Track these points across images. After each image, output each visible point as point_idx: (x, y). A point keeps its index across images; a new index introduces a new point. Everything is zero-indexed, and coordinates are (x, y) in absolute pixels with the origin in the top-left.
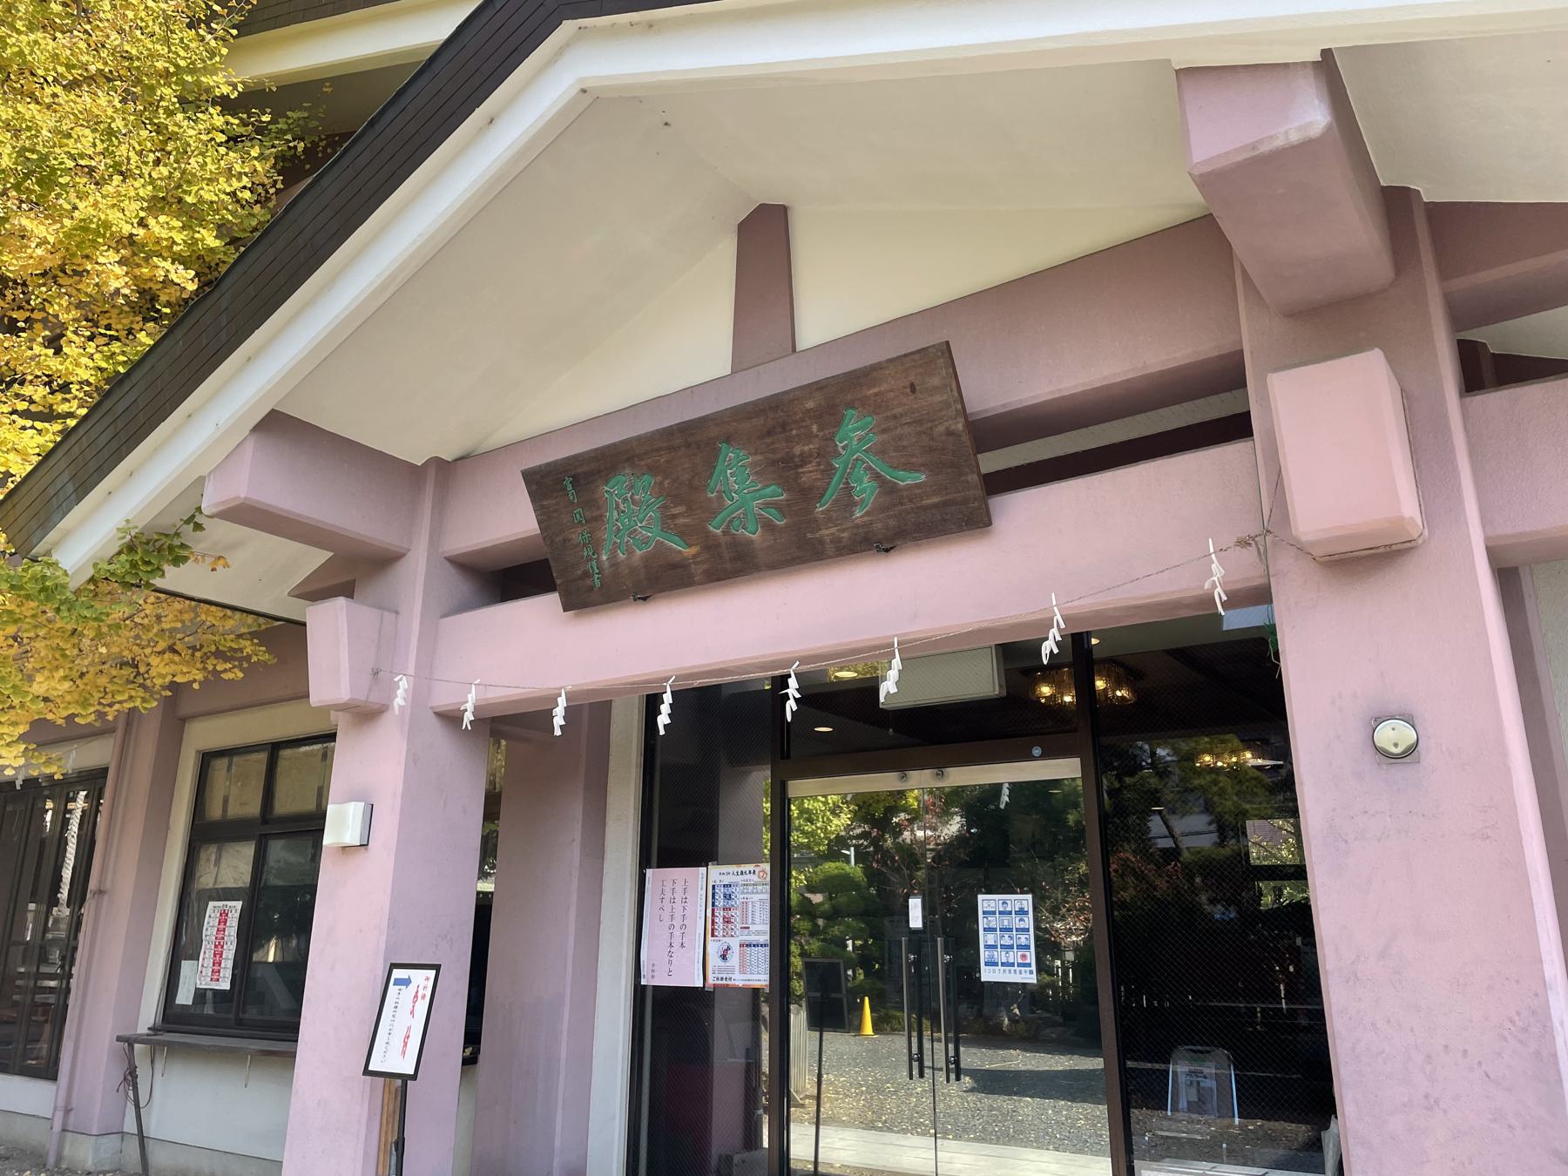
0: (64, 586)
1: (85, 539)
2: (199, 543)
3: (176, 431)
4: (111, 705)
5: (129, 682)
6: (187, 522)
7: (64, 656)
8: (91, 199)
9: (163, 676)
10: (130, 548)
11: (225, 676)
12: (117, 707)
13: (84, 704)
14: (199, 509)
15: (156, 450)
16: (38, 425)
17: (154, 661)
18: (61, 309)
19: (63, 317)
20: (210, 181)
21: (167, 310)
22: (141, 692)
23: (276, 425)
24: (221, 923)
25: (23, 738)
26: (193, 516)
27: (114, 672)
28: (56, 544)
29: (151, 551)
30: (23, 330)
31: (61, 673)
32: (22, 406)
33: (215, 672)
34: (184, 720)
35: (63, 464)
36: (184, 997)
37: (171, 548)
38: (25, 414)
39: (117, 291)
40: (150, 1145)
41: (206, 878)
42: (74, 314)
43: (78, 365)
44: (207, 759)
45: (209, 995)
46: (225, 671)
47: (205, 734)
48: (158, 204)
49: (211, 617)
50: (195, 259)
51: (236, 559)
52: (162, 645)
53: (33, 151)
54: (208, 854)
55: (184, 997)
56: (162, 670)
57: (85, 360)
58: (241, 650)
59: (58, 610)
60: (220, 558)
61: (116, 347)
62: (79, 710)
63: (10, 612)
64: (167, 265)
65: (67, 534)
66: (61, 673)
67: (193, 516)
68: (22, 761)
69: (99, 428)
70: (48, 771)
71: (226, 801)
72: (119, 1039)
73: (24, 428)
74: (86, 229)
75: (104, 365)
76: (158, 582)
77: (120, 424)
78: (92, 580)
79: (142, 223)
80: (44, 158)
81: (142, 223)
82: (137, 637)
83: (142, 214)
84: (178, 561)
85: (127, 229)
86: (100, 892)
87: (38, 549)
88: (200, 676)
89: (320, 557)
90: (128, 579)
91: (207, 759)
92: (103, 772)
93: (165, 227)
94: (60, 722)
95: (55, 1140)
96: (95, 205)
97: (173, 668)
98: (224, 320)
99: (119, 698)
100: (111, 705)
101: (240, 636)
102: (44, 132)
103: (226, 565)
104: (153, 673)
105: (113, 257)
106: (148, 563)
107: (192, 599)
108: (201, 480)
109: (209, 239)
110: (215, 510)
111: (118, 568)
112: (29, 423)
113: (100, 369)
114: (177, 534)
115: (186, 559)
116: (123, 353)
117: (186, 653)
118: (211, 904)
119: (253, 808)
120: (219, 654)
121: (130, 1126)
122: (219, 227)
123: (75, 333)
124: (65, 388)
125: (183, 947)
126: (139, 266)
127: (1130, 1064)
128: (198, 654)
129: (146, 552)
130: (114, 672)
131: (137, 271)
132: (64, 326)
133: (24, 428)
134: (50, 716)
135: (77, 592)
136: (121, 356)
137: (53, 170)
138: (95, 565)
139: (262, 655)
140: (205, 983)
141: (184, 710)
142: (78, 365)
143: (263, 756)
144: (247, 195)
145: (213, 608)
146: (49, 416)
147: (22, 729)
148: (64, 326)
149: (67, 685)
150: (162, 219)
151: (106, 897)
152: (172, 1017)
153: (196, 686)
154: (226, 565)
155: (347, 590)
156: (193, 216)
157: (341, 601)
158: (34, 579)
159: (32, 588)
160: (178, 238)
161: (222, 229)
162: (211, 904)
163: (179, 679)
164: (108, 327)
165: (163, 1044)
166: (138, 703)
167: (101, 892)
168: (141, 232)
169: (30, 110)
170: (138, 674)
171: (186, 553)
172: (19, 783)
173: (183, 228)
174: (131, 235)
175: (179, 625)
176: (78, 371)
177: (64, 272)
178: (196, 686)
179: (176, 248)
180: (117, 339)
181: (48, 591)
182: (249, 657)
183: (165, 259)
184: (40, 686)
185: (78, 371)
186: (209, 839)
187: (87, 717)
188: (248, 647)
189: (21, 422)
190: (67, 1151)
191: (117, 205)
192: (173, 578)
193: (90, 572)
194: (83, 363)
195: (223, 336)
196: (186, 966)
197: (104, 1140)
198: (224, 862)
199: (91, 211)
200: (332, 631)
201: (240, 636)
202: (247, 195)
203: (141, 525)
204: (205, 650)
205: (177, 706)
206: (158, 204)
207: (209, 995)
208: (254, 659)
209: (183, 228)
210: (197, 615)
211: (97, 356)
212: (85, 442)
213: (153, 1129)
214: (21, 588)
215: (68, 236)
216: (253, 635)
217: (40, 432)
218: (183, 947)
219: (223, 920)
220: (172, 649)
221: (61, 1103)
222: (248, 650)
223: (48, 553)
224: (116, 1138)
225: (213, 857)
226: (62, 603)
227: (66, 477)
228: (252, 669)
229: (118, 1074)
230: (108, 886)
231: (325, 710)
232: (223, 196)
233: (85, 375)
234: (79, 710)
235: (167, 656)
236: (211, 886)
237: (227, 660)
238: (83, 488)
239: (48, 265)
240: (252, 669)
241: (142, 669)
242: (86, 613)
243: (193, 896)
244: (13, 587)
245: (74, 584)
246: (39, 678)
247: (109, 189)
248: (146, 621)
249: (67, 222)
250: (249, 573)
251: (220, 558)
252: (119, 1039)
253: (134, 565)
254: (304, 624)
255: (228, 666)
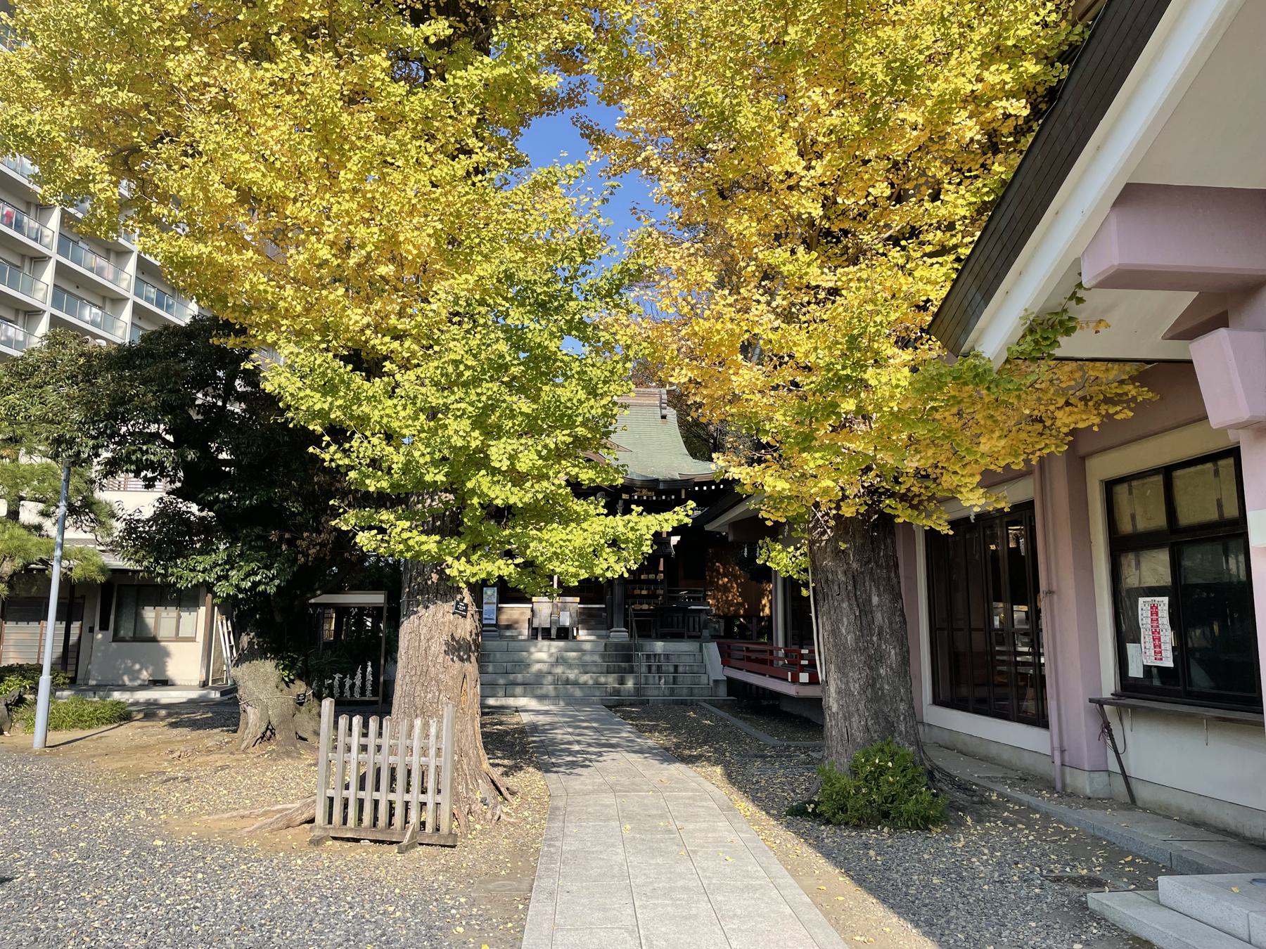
0: (990, 370)
1: (997, 332)
2: (1080, 313)
3: (1048, 230)
4: (1033, 453)
5: (1041, 434)
6: (1071, 298)
7: (995, 421)
8: (941, 76)
9: (1065, 425)
10: (1031, 330)
11: (1118, 417)
12: (1038, 453)
13: (1017, 455)
14: (1080, 285)
15: (1036, 248)
16: (940, 259)
17: (1059, 414)
18: (937, 170)
19: (939, 175)
20: (1022, 21)
21: (1011, 139)
22: (1053, 440)
23: (1132, 195)
24: (1154, 615)
25: (980, 485)
26: (1075, 293)
27: (1029, 428)
28: (976, 341)
29: (1047, 328)
30: (913, 196)
31: (997, 434)
32: (928, 249)
33: (1109, 416)
34: (1083, 458)
35: (970, 280)
36: (1135, 671)
37: (1061, 323)
38: (930, 255)
39: (972, 140)
40: (1134, 784)
41: (1131, 579)
42: (947, 169)
43: (956, 206)
44: (1110, 486)
45: (1155, 671)
46: (1117, 413)
47: (1103, 467)
48: (986, 60)
49: (1094, 371)
50: (1025, 90)
51: (1113, 318)
52: (1061, 402)
53: (895, 61)
54: (1128, 561)
55: (1135, 671)
56: (1065, 420)
57: (960, 201)
58: (1126, 394)
59: (988, 389)
60: (1100, 321)
61: (979, 183)
62: (1012, 459)
63: (954, 397)
64: (1004, 103)
65: (982, 332)
66: (997, 434)
67: (1075, 293)
68: (983, 501)
69: (990, 246)
70: (999, 507)
71: (1133, 518)
72: (1091, 701)
73: (932, 265)
74: (943, 102)
75: (973, 200)
76: (1058, 352)
77: (1005, 237)
78: (1007, 361)
79: (980, 79)
80: (904, 62)
81: (980, 79)
82: (1039, 399)
83: (978, 72)
84: (1069, 331)
85: (969, 88)
86: (1050, 592)
87: (965, 349)
88: (1097, 420)
89: (1187, 298)
90: (1034, 354)
91: (1110, 486)
92: (1029, 505)
93: (998, 75)
94: (999, 470)
95: (1058, 769)
96: (946, 80)
97: (1071, 419)
98: (1071, 124)
99: (1038, 447)
100: (1033, 453)
101: (1122, 382)
102: (900, 43)
103: (1108, 326)
104: (1058, 423)
105: (964, 114)
106: (1046, 339)
107: (1081, 360)
108: (1077, 262)
109: (1031, 67)
110: (1094, 282)
111: (1027, 346)
112: (934, 260)
113: (970, 204)
114: (1065, 311)
115: (1074, 329)
116: (984, 185)
117: (1081, 405)
118: (1141, 600)
119: (1158, 520)
120: (1108, 401)
121: (1113, 766)
122: (1035, 54)
123: (950, 183)
124: (951, 226)
125: (1125, 633)
126: (982, 113)
127: (491, 702)
128: (1091, 403)
129: (1044, 330)
130: (1029, 428)
131: (982, 119)
132: (939, 182)
133: (932, 265)
134: (992, 467)
135: (999, 372)
136: (985, 189)
137: (912, 68)
138: (1009, 349)
139: (1145, 394)
140: (1151, 661)
141: (1082, 450)
142: (956, 206)
143: (1159, 479)
144: (1054, 17)
145: (1098, 364)
146: (943, 251)
147: (978, 478)
148: (939, 182)
149: (1003, 442)
150: (993, 68)
151: (1055, 597)
152: (1128, 686)
153: (1096, 429)
154: (1108, 326)
155: (1221, 321)
156: (1014, 55)
157: (1222, 332)
158: (969, 369)
159: (969, 376)
160: (1007, 77)
161: (1040, 57)
162: (1141, 600)
163: (1081, 425)
164: (970, 170)
165: (1126, 706)
166: (1053, 448)
167: (1050, 592)
168: (980, 86)
169: (886, 32)
170: (1045, 427)
171: (1072, 324)
172: (972, 518)
173: (1010, 68)
174: (973, 91)
175: (1073, 383)
176: (958, 211)
177: (935, 138)
178: (1096, 429)
179: (1007, 87)
180: (976, 177)
181: (979, 376)
182: (1134, 398)
183: (1001, 100)
184: (985, 446)
185: (958, 211)
186: (1127, 550)
187: (1019, 465)
188: (1131, 390)
189: (929, 261)
190: (1068, 780)
191: (959, 77)
192: (1068, 346)
193: (1005, 356)
194: (958, 202)
195: (1073, 138)
196: (1131, 648)
197: (1096, 775)
198: (1144, 566)
199: (945, 86)
200: (1219, 362)
201: (1122, 382)
202: (1054, 17)
203: (1036, 310)
204: (1095, 399)
205: (1079, 450)
206: (986, 60)
207: (1155, 671)
208: (1140, 399)
209: (1010, 68)
210: (1085, 373)
211: (967, 195)
212: (982, 260)
213: (1132, 771)
214: (959, 378)
215: (932, 112)
216: (1133, 379)
217: (941, 264)
218: (1125, 633)
219: (1154, 610)
220: (1068, 404)
221: (1056, 744)
222: (1134, 393)
223: (973, 349)
224: (1104, 776)
225: (1133, 563)
226: (991, 382)
227: (973, 290)
228: (1140, 407)
229: (1096, 729)
230: (1054, 588)
231: (1223, 431)
232: (1035, 27)
233: (962, 212)
234: (1012, 459)
235: (1067, 409)
236: (1136, 585)
237: (1115, 404)
238: (988, 295)
239: (922, 140)
240: (1140, 407)
241: (1048, 423)
242: (1009, 386)
243: (1124, 594)
244: (954, 378)
245: (996, 366)
246: (983, 440)
247: (953, 62)
248: (1043, 386)
249: (929, 103)
250: (1133, 327)
251: (1100, 321)
252: (1091, 701)
253: (1036, 342)
254: (1190, 362)
255: (1118, 408)
